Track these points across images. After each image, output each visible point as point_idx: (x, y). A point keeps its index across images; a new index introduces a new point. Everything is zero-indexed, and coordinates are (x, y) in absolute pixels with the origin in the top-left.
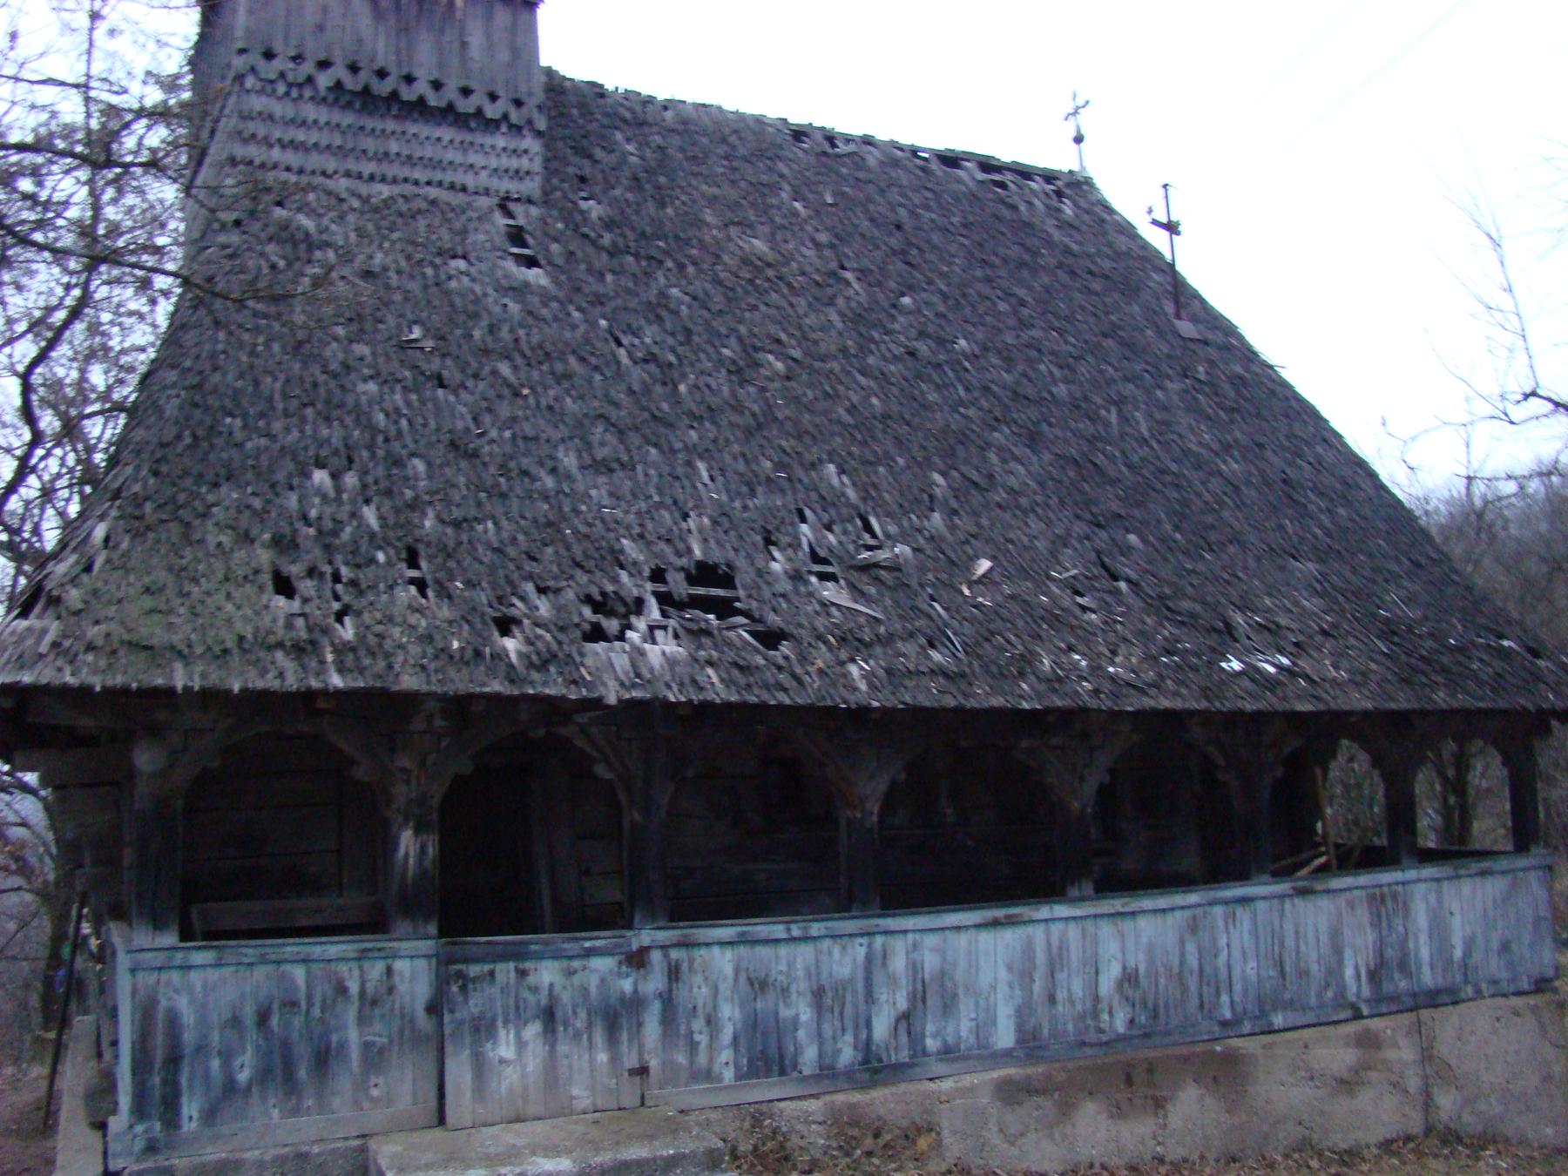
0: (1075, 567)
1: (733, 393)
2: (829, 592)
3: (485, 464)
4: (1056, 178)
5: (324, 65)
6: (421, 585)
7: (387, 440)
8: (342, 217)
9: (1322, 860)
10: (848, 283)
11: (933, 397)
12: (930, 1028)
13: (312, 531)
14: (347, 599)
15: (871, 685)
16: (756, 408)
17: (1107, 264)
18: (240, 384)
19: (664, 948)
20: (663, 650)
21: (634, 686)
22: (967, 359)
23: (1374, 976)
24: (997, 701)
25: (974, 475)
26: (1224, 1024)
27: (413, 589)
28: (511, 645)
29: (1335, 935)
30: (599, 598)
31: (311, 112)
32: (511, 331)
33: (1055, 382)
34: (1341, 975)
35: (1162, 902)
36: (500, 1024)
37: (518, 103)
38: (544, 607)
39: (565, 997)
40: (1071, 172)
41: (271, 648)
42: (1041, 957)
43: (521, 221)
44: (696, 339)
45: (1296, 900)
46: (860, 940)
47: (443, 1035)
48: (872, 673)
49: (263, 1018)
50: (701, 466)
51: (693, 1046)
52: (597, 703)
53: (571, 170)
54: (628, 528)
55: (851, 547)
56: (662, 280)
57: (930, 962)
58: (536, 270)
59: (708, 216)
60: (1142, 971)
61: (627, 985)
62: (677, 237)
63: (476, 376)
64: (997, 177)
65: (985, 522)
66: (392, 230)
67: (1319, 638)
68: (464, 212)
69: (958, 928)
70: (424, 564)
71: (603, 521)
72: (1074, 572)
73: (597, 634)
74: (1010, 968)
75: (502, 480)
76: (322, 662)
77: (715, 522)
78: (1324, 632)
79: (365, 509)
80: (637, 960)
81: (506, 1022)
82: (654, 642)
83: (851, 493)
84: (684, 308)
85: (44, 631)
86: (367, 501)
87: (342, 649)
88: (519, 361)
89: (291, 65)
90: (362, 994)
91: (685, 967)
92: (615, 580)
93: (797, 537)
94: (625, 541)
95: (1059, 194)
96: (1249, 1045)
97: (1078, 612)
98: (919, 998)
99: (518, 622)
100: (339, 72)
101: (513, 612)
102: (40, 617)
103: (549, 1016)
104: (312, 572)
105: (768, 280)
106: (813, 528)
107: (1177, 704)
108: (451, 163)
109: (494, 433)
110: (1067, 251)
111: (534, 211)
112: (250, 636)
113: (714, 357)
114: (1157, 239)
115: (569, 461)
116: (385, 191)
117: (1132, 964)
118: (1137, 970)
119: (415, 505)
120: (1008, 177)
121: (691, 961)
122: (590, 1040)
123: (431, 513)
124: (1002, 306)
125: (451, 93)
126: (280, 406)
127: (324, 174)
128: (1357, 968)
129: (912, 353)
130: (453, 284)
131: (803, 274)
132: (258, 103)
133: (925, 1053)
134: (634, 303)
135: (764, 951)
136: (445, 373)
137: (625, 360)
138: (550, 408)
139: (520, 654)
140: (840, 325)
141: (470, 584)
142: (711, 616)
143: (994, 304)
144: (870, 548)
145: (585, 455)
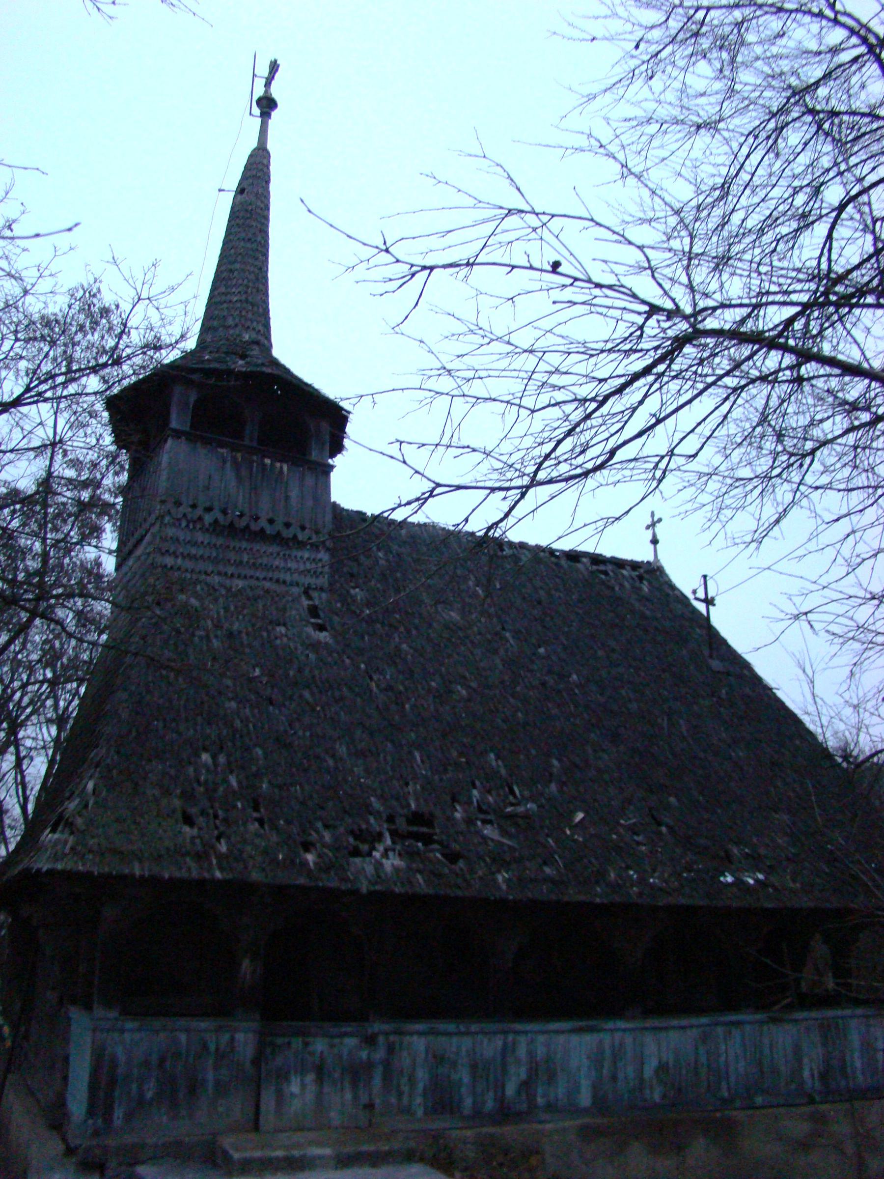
0: (635, 817)
1: (437, 710)
2: (489, 831)
3: (295, 752)
4: (640, 567)
5: (209, 509)
6: (261, 822)
7: (241, 736)
8: (216, 600)
9: (788, 1000)
10: (507, 641)
11: (555, 711)
12: (540, 1091)
13: (202, 789)
14: (222, 829)
15: (508, 886)
16: (449, 719)
17: (667, 624)
18: (161, 701)
19: (386, 1034)
20: (393, 862)
21: (376, 883)
22: (577, 686)
23: (824, 1076)
24: (581, 898)
25: (577, 760)
26: (724, 1101)
27: (257, 825)
28: (310, 857)
29: (797, 1049)
30: (358, 833)
31: (200, 537)
32: (311, 671)
33: (630, 701)
35: (684, 1022)
36: (292, 1072)
38: (327, 837)
40: (648, 562)
41: (183, 855)
42: (608, 1052)
43: (317, 602)
44: (416, 676)
45: (771, 1025)
47: (260, 1078)
48: (510, 880)
49: (162, 1060)
50: (417, 755)
51: (400, 1094)
52: (356, 892)
53: (345, 570)
54: (375, 790)
55: (501, 804)
56: (397, 639)
57: (541, 1051)
58: (325, 634)
59: (425, 597)
60: (671, 1063)
61: (364, 1055)
62: (406, 612)
63: (291, 698)
64: (602, 567)
65: (581, 789)
66: (244, 608)
67: (784, 863)
68: (284, 597)
70: (262, 810)
71: (360, 786)
72: (634, 820)
73: (356, 853)
74: (588, 1058)
75: (305, 761)
76: (211, 864)
77: (423, 788)
78: (788, 859)
79: (230, 777)
80: (370, 1040)
81: (296, 1072)
82: (388, 858)
83: (503, 771)
84: (409, 657)
85: (66, 842)
86: (231, 772)
87: (220, 856)
88: (315, 690)
89: (190, 510)
90: (217, 1049)
91: (397, 1046)
92: (368, 822)
93: (470, 797)
94: (372, 799)
95: (641, 578)
96: (740, 1115)
97: (634, 846)
98: (533, 1071)
99: (313, 844)
100: (217, 514)
101: (311, 839)
102: (62, 832)
103: (321, 1071)
104: (203, 812)
105: (459, 638)
106: (480, 792)
107: (690, 902)
108: (277, 567)
109: (300, 733)
110: (643, 616)
111: (324, 596)
112: (172, 848)
113: (426, 687)
114: (701, 607)
115: (342, 750)
116: (240, 583)
117: (664, 1059)
118: (667, 1063)
119: (258, 775)
120: (609, 568)
121: (401, 1044)
123: (266, 780)
124: (600, 653)
125: (279, 526)
126: (183, 716)
127: (206, 573)
128: (811, 1069)
129: (544, 684)
130: (278, 642)
131: (480, 633)
132: (171, 532)
133: (536, 1106)
134: (380, 654)
135: (443, 1039)
136: (274, 696)
137: (375, 689)
138: (332, 718)
139: (315, 863)
140: (501, 667)
141: (288, 822)
142: (420, 844)
143: (596, 652)
144: (512, 805)
145: (351, 747)
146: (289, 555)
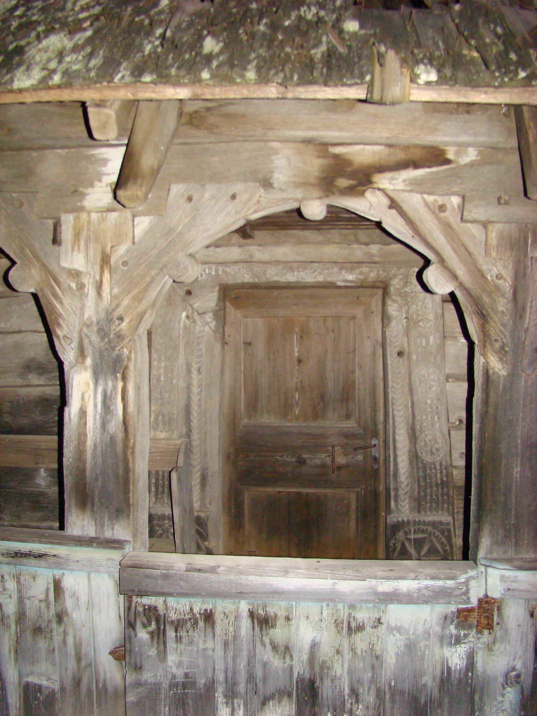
34: (156, 316)
36: (220, 698)
90: (21, 616)
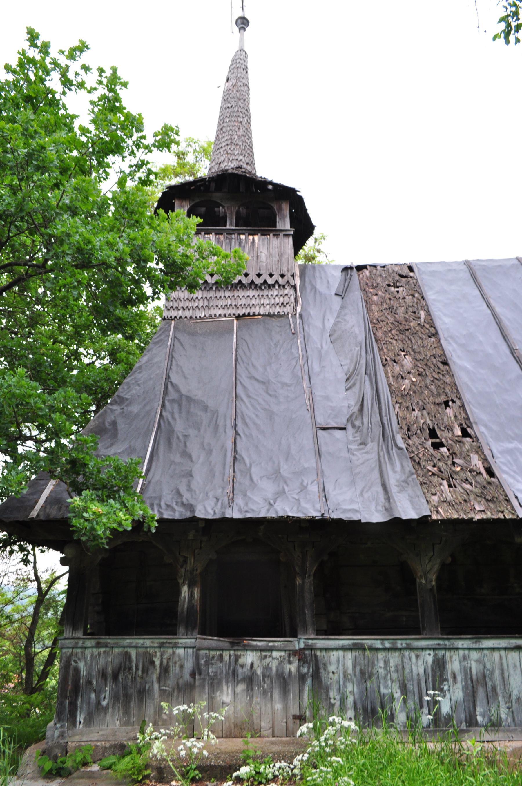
37: (282, 276)
39: (259, 671)
46: (428, 652)
69: (493, 649)
122: (272, 695)
146: (262, 296)
